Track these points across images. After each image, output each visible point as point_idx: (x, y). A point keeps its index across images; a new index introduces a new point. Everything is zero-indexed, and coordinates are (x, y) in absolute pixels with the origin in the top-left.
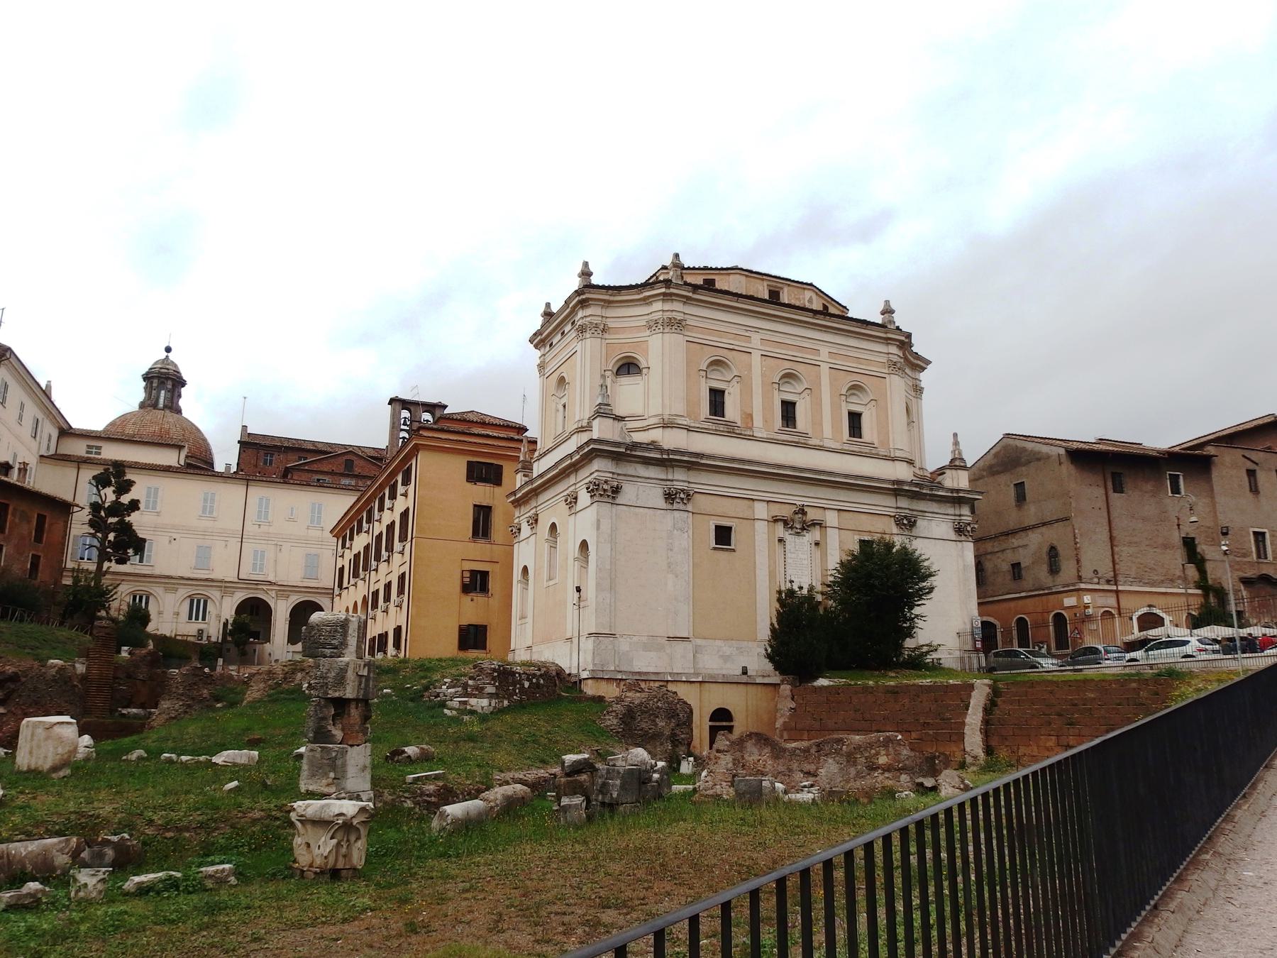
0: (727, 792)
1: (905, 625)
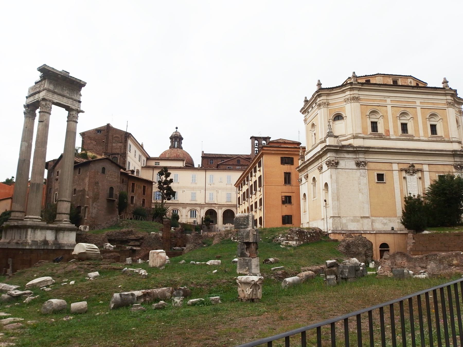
0: (389, 274)
1: (461, 208)
